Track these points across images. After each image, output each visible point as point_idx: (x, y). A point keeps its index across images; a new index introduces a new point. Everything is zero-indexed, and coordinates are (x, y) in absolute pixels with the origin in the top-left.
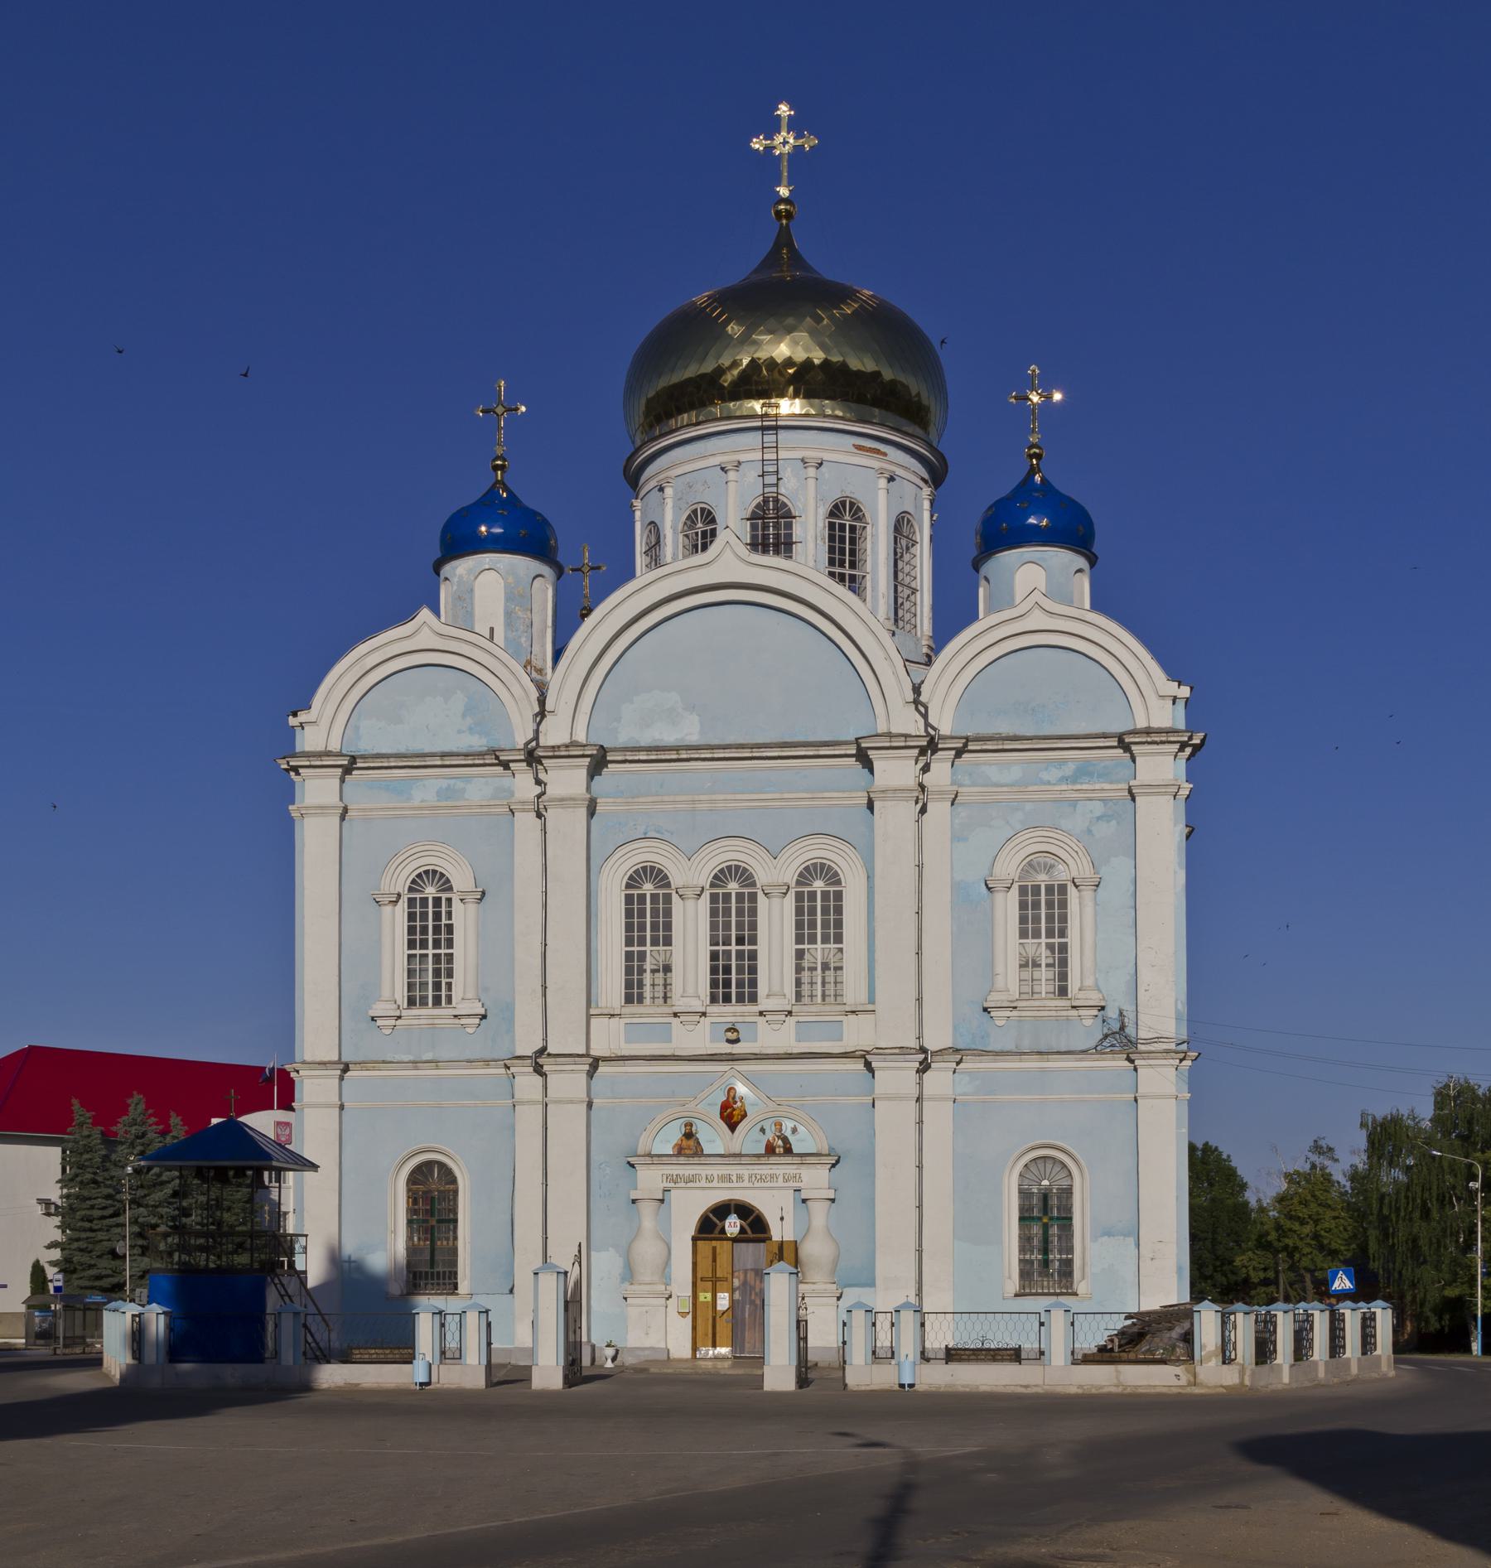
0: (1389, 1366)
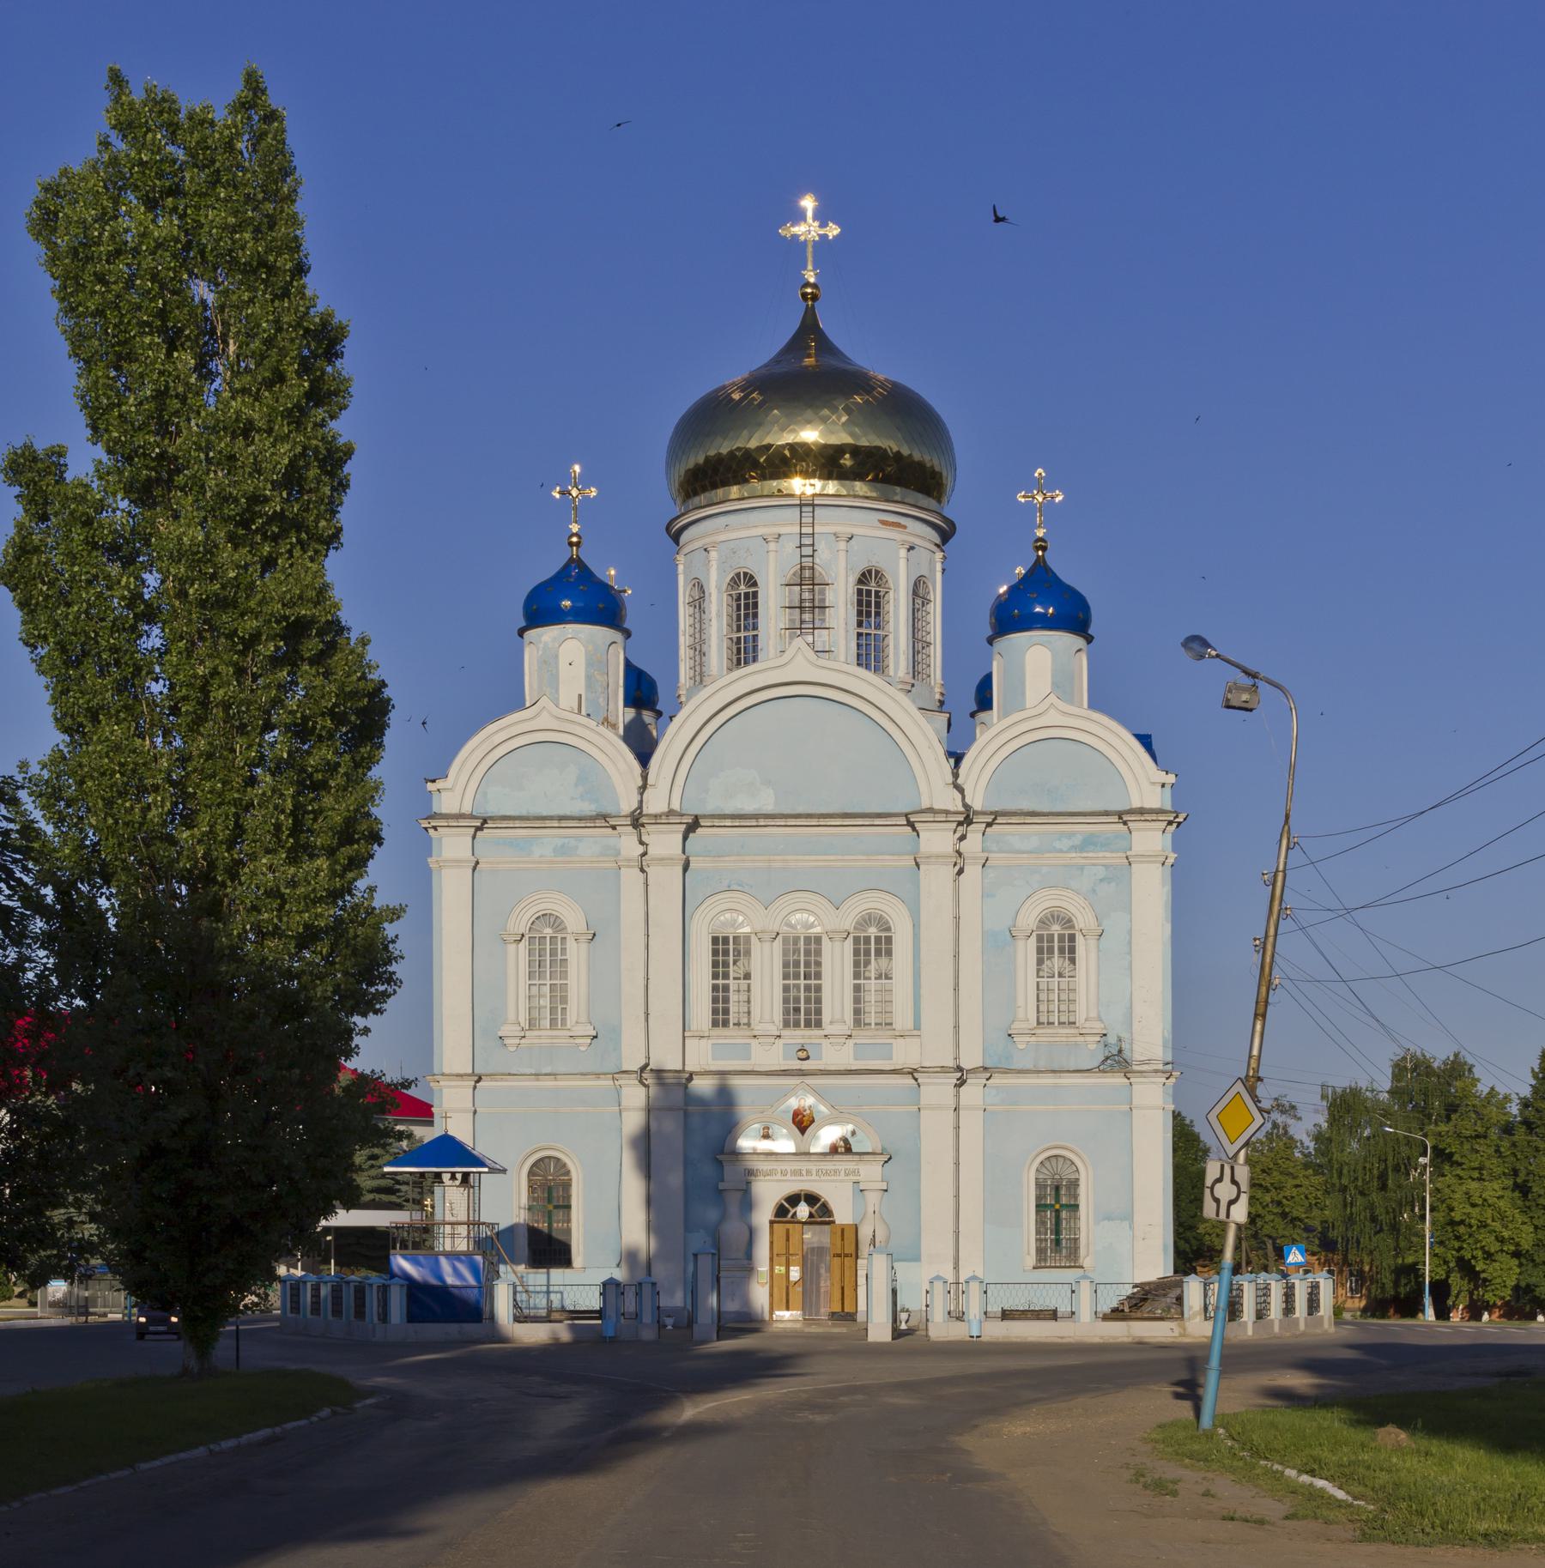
0: (1330, 1325)
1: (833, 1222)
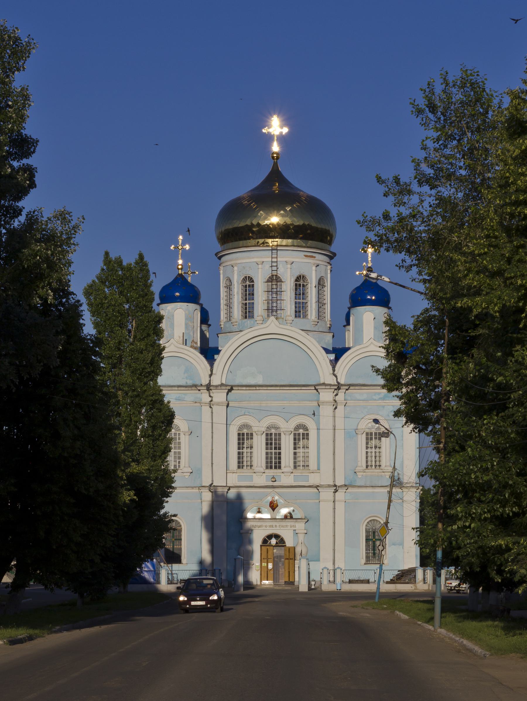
1: (286, 546)
